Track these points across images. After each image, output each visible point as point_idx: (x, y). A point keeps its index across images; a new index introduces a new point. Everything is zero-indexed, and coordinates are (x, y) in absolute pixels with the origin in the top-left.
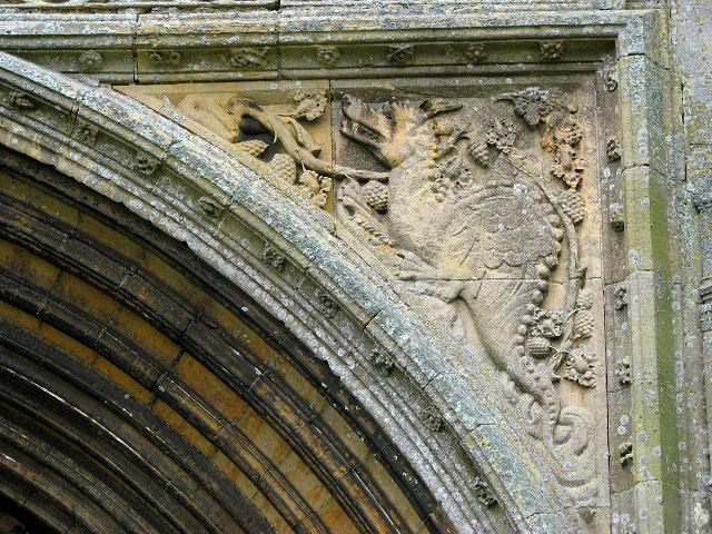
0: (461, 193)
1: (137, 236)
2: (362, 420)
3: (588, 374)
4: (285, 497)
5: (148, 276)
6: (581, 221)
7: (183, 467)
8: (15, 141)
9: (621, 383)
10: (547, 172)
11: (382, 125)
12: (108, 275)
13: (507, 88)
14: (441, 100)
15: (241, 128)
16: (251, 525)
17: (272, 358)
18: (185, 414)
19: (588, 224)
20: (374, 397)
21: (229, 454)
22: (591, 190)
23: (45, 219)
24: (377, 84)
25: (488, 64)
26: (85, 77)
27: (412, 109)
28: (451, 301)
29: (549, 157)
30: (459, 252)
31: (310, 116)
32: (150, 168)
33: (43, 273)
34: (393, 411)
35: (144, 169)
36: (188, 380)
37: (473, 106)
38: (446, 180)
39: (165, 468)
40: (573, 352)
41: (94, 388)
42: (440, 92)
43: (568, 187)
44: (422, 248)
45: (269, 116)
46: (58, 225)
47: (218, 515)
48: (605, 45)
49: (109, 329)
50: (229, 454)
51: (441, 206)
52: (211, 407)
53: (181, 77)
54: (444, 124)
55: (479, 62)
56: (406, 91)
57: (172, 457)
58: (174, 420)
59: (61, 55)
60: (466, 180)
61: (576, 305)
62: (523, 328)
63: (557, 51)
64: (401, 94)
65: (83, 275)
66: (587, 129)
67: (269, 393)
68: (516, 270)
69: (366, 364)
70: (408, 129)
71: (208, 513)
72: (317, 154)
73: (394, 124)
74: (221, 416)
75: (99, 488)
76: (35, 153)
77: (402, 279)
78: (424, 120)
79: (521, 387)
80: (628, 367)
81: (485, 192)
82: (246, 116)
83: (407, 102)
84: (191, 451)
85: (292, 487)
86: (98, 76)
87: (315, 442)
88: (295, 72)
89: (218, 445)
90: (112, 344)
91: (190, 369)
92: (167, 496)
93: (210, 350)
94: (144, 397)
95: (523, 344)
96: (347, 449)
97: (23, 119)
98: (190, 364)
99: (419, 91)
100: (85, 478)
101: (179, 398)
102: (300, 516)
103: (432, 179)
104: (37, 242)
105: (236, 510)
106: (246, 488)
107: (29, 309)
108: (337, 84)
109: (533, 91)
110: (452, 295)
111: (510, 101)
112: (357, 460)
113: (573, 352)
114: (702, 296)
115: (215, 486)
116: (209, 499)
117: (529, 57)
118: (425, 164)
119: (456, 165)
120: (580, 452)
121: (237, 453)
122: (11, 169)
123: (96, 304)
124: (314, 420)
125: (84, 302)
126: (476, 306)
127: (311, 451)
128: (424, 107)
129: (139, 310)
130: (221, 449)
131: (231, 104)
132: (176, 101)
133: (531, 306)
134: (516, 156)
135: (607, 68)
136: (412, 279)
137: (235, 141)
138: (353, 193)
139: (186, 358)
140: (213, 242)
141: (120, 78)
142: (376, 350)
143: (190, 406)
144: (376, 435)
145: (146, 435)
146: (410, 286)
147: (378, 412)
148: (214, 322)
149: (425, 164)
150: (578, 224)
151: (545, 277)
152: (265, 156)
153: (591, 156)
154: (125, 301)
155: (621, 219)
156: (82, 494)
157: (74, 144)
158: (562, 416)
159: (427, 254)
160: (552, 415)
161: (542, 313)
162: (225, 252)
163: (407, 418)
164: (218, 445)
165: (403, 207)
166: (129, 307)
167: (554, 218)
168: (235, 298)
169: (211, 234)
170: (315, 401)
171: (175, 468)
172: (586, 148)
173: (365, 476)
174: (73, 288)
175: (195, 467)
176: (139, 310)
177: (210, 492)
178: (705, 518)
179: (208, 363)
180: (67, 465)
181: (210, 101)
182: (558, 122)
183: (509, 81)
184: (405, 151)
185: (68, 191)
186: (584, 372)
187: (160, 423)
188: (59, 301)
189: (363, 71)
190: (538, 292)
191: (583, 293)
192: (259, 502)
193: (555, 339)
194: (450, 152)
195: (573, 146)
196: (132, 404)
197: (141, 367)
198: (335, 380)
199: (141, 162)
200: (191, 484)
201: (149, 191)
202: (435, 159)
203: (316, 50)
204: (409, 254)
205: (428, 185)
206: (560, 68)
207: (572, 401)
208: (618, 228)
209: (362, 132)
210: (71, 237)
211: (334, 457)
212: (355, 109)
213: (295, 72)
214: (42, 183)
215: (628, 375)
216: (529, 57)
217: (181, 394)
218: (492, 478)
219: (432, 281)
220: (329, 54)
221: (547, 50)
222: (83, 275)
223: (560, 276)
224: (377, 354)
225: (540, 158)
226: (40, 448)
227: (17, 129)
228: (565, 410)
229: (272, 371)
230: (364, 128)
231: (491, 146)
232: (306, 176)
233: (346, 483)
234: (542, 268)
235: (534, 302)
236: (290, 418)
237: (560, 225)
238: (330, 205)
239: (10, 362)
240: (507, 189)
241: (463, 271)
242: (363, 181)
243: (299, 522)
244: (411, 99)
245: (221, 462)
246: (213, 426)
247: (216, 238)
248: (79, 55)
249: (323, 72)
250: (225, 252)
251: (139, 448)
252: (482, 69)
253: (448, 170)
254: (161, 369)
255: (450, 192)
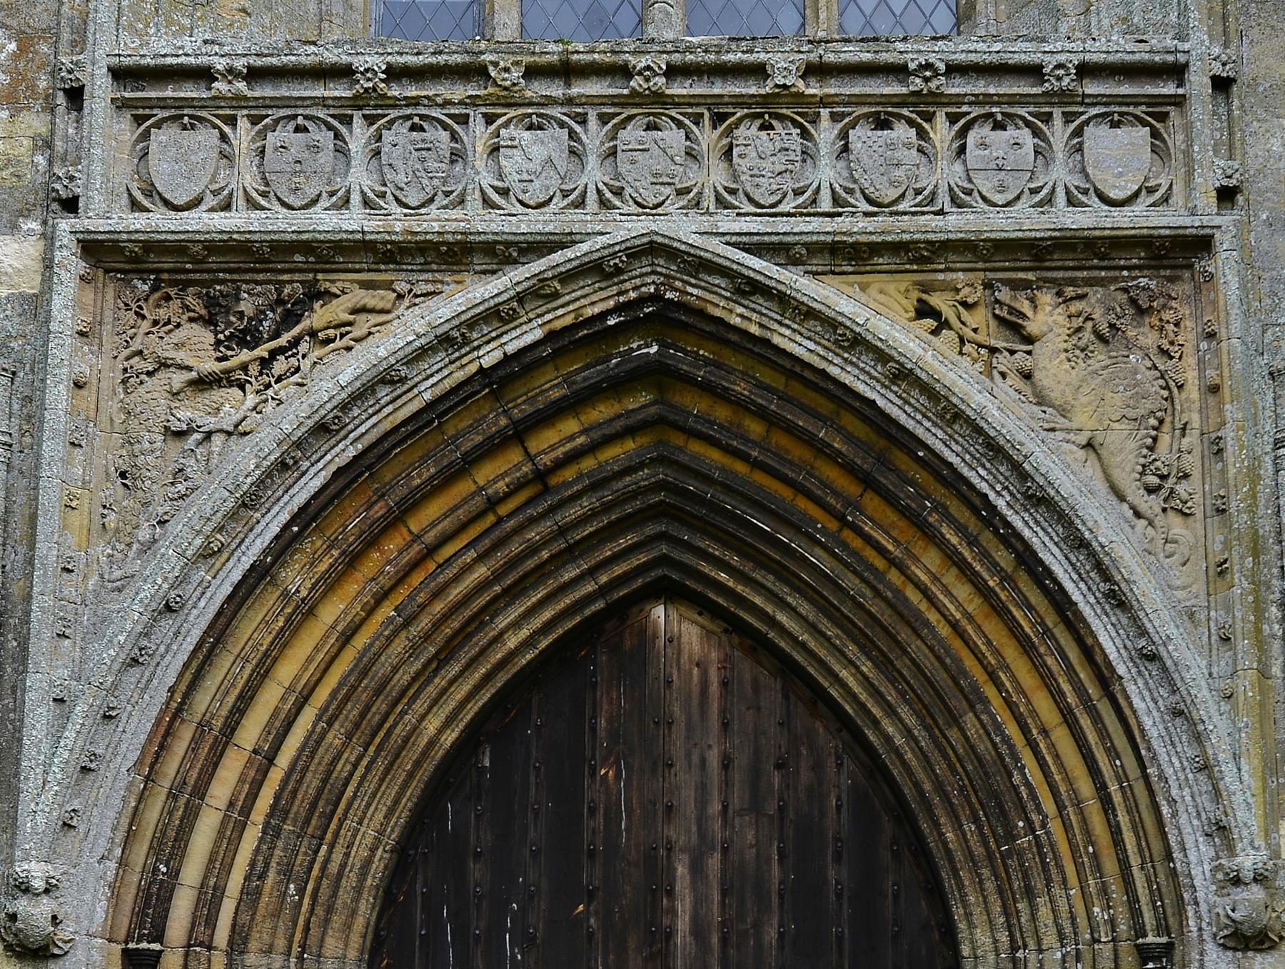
0: (1089, 362)
1: (835, 396)
2: (1013, 540)
3: (1189, 504)
4: (946, 601)
5: (840, 430)
6: (1182, 385)
7: (864, 580)
8: (738, 320)
9: (1218, 510)
10: (1155, 347)
11: (1025, 307)
12: (810, 428)
13: (1124, 279)
14: (1071, 288)
15: (916, 310)
16: (917, 624)
17: (940, 492)
18: (868, 539)
19: (1188, 387)
20: (1026, 523)
21: (902, 569)
22: (1190, 360)
23: (760, 385)
24: (1021, 275)
25: (1110, 259)
26: (789, 267)
27: (1049, 296)
28: (1084, 447)
29: (1156, 334)
30: (1089, 408)
31: (970, 300)
32: (848, 340)
33: (755, 428)
34: (1041, 533)
35: (843, 341)
36: (869, 511)
37: (1096, 294)
38: (1077, 352)
39: (849, 582)
40: (1177, 487)
41: (794, 519)
42: (1073, 282)
43: (1172, 358)
44: (1060, 406)
45: (936, 300)
46: (769, 389)
47: (890, 616)
48: (1202, 244)
49: (808, 473)
50: (902, 569)
51: (1074, 372)
52: (887, 533)
53: (868, 268)
54: (1076, 307)
55: (1103, 257)
56: (1046, 280)
57: (855, 572)
58: (857, 543)
59: (775, 250)
60: (1092, 352)
61: (1180, 451)
62: (1140, 468)
63: (1165, 248)
64: (1041, 284)
65: (790, 429)
66: (1187, 312)
67: (937, 520)
68: (1133, 423)
69: (1019, 496)
70: (1047, 311)
71: (882, 616)
72: (975, 330)
73: (1036, 307)
74: (895, 540)
75: (795, 597)
76: (754, 329)
77: (1045, 430)
78: (1060, 304)
79: (1138, 515)
80: (1224, 497)
81: (1108, 362)
82: (920, 300)
83: (1045, 290)
84: (871, 568)
85: (950, 593)
86: (801, 267)
87: (974, 558)
88: (958, 265)
89: (893, 562)
90: (812, 485)
91: (872, 503)
92: (850, 603)
93: (890, 487)
94: (833, 525)
95: (1139, 480)
96: (998, 564)
97: (746, 303)
98: (871, 499)
99: (1053, 281)
100: (784, 591)
101: (864, 526)
102: (958, 616)
103: (1066, 351)
104: (754, 403)
105: (906, 612)
106: (913, 595)
107: (744, 457)
108: (990, 275)
109: (1143, 281)
110: (1084, 443)
111: (1125, 290)
112: (1006, 572)
113: (1177, 487)
114: (1276, 444)
115: (889, 594)
116: (883, 605)
117: (1142, 254)
118: (1060, 339)
119: (1085, 341)
120: (1184, 564)
121: (909, 568)
122: (734, 343)
123: (798, 452)
124: (972, 542)
125: (787, 452)
126: (1103, 452)
127: (970, 565)
128: (1059, 294)
129: (832, 456)
130: (896, 566)
131: (907, 290)
132: (864, 288)
133: (1145, 451)
134: (1131, 333)
135: (1203, 263)
136: (1053, 430)
137: (910, 320)
138: (1005, 361)
139: (869, 495)
140: (896, 400)
141: (820, 269)
142: (1029, 484)
143: (872, 532)
144: (1024, 551)
145: (835, 556)
146: (1051, 435)
147: (1027, 533)
148: (894, 466)
149: (1060, 339)
150: (1180, 387)
151: (1155, 429)
152: (935, 332)
153: (1188, 336)
154: (822, 450)
155: (1217, 382)
156: (477, 689)
157: (787, 322)
158: (1170, 536)
159: (1064, 410)
160: (1163, 536)
161: (1153, 457)
162: (906, 408)
163: (1051, 538)
164: (893, 562)
165: (1044, 373)
166: (826, 454)
167: (1161, 382)
168: (913, 445)
169: (895, 393)
170: (973, 525)
171: (857, 581)
172: (1186, 328)
173: (1012, 584)
174: (781, 440)
175: (873, 580)
176: (832, 456)
177: (885, 600)
178: (1279, 615)
179: (890, 499)
180: (769, 581)
181: (891, 288)
182: (1164, 306)
183: (1125, 273)
184: (1045, 329)
185: (780, 361)
186: (1186, 503)
187: (845, 546)
188: (768, 450)
189: (1013, 265)
190: (1151, 440)
191: (1185, 441)
192: (923, 606)
193: (1163, 477)
194: (1079, 330)
195: (1176, 325)
196: (823, 531)
197: (833, 502)
198: (993, 509)
199: (840, 335)
200: (869, 593)
201: (845, 360)
202: (1068, 335)
203: (976, 246)
204: (1049, 410)
205: (1063, 356)
206: (1165, 262)
207: (1177, 526)
208: (1215, 389)
209: (1010, 313)
210: (780, 398)
211: (988, 570)
212: (1004, 294)
213: (958, 265)
214: (758, 354)
215: (1224, 504)
216: (1142, 254)
217: (866, 524)
218: (1123, 585)
219: (1068, 431)
220: (987, 250)
221: (1158, 248)
222: (790, 429)
223: (1167, 427)
224: (1029, 488)
225: (1150, 335)
226: (747, 568)
227: (740, 310)
228: (1171, 532)
229: (939, 503)
230: (1012, 310)
231: (1112, 326)
232: (968, 348)
233: (997, 589)
234: (1153, 422)
235: (1147, 448)
236: (954, 540)
237: (1167, 387)
238: (989, 371)
239: (727, 500)
240: (1126, 359)
241: (1092, 424)
242: (1012, 352)
243: (958, 621)
244: (1048, 288)
245: (894, 576)
246: (890, 547)
247: (900, 397)
248: (788, 250)
249: (980, 265)
250: (906, 408)
251: (829, 566)
252: (1105, 263)
253: (1079, 344)
254: (848, 503)
255: (1080, 361)
